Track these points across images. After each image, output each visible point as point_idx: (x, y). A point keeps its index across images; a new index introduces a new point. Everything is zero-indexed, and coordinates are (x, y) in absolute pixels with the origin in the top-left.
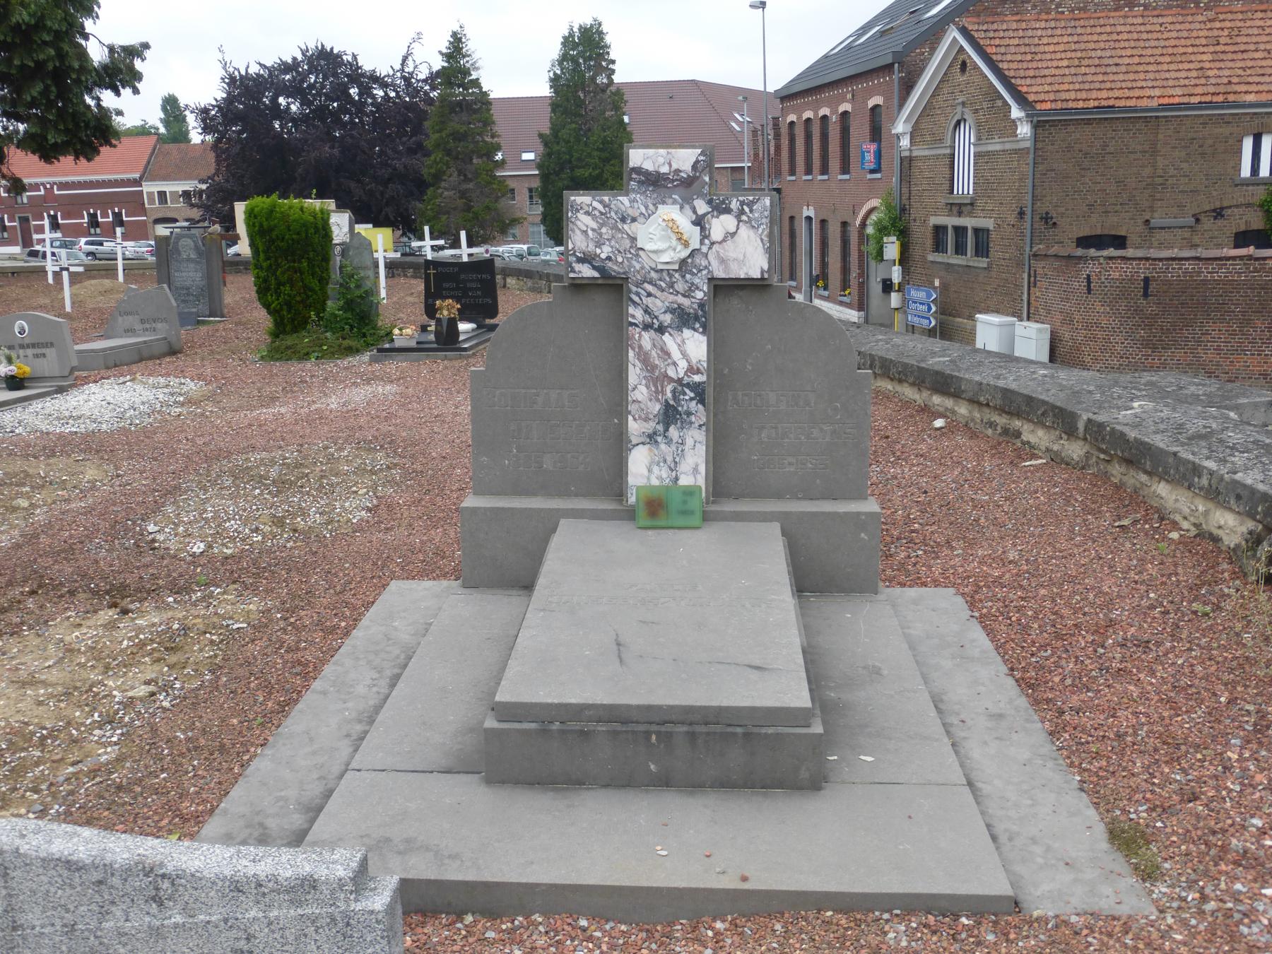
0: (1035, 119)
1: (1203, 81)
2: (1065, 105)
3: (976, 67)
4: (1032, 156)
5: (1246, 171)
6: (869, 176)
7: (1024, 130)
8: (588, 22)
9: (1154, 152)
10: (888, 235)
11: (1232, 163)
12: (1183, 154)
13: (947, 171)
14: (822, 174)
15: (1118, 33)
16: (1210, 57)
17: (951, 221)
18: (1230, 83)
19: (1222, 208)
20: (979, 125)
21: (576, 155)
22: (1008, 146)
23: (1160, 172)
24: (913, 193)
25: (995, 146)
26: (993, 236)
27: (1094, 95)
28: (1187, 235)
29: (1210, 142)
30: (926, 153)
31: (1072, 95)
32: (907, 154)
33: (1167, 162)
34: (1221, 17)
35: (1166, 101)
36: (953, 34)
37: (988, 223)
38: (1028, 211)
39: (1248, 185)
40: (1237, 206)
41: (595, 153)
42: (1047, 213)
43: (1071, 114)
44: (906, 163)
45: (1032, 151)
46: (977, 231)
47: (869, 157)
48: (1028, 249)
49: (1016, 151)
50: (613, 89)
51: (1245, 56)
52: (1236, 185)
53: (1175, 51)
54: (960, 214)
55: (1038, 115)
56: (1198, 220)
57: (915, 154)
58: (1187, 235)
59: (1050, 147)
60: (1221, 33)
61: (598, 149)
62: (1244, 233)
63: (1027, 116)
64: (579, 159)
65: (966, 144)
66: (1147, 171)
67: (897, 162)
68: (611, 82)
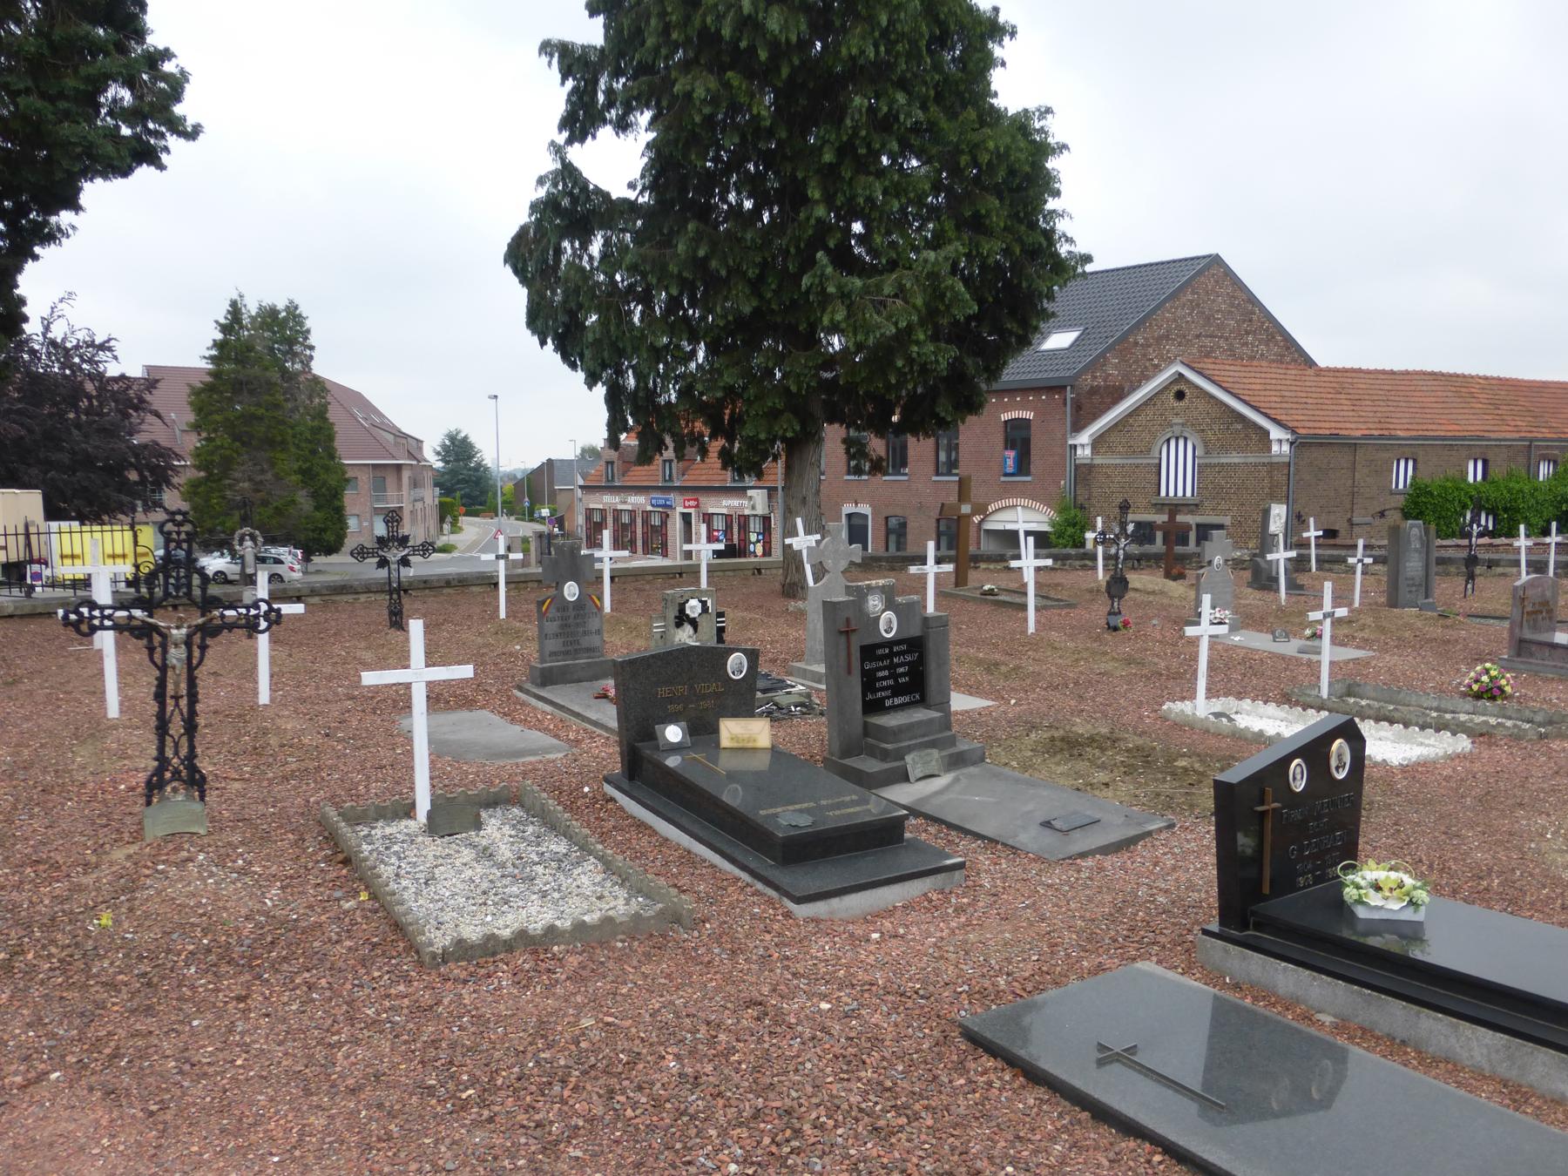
67: (1069, 469)
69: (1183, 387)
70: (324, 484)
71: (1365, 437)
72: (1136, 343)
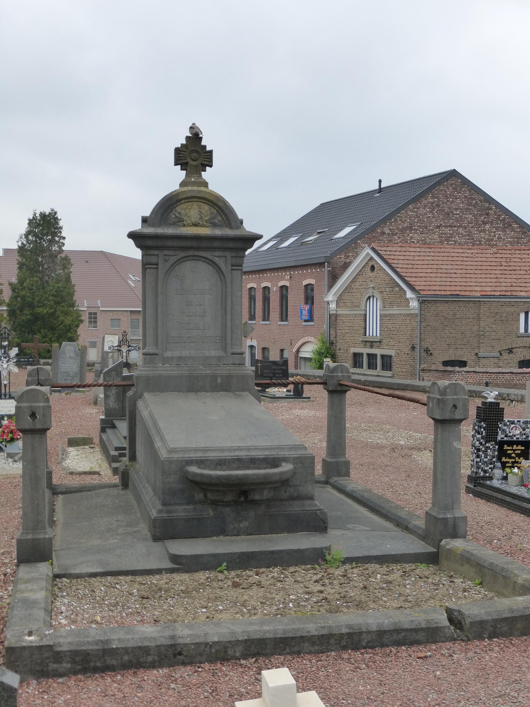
0: (421, 299)
1: (499, 284)
2: (435, 293)
3: (382, 269)
4: (419, 318)
5: (522, 330)
6: (304, 323)
7: (414, 304)
8: (47, 211)
9: (479, 319)
10: (326, 357)
11: (516, 326)
12: (492, 320)
13: (362, 323)
14: (264, 320)
15: (452, 257)
16: (500, 272)
17: (366, 351)
18: (512, 286)
19: (512, 348)
20: (384, 300)
21: (37, 299)
22: (403, 312)
23: (482, 329)
24: (338, 334)
25: (395, 311)
26: (394, 359)
27: (448, 288)
28: (496, 361)
29: (505, 315)
30: (348, 312)
31: (438, 288)
32: (334, 312)
33: (485, 324)
34: (500, 252)
35: (484, 293)
36: (367, 251)
37: (392, 353)
38: (418, 347)
39: (523, 337)
40: (519, 348)
41: (51, 298)
42: (427, 348)
43: (438, 297)
44: (333, 318)
45: (419, 315)
46: (383, 356)
47: (305, 313)
48: (418, 367)
49: (408, 315)
50: (63, 255)
51: (515, 272)
52: (518, 337)
53: (482, 268)
54: (372, 347)
55: (422, 297)
56: (501, 354)
57: (339, 313)
58: (496, 361)
59: (428, 314)
60: (502, 260)
61: (53, 295)
62: (523, 361)
63: (417, 297)
64: (39, 302)
65: (374, 310)
66: (475, 328)
67: (327, 317)
68: (61, 251)
69: (374, 263)
70: (63, 322)
71: (483, 296)
72: (383, 233)
